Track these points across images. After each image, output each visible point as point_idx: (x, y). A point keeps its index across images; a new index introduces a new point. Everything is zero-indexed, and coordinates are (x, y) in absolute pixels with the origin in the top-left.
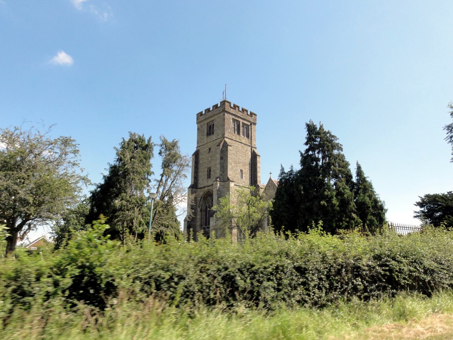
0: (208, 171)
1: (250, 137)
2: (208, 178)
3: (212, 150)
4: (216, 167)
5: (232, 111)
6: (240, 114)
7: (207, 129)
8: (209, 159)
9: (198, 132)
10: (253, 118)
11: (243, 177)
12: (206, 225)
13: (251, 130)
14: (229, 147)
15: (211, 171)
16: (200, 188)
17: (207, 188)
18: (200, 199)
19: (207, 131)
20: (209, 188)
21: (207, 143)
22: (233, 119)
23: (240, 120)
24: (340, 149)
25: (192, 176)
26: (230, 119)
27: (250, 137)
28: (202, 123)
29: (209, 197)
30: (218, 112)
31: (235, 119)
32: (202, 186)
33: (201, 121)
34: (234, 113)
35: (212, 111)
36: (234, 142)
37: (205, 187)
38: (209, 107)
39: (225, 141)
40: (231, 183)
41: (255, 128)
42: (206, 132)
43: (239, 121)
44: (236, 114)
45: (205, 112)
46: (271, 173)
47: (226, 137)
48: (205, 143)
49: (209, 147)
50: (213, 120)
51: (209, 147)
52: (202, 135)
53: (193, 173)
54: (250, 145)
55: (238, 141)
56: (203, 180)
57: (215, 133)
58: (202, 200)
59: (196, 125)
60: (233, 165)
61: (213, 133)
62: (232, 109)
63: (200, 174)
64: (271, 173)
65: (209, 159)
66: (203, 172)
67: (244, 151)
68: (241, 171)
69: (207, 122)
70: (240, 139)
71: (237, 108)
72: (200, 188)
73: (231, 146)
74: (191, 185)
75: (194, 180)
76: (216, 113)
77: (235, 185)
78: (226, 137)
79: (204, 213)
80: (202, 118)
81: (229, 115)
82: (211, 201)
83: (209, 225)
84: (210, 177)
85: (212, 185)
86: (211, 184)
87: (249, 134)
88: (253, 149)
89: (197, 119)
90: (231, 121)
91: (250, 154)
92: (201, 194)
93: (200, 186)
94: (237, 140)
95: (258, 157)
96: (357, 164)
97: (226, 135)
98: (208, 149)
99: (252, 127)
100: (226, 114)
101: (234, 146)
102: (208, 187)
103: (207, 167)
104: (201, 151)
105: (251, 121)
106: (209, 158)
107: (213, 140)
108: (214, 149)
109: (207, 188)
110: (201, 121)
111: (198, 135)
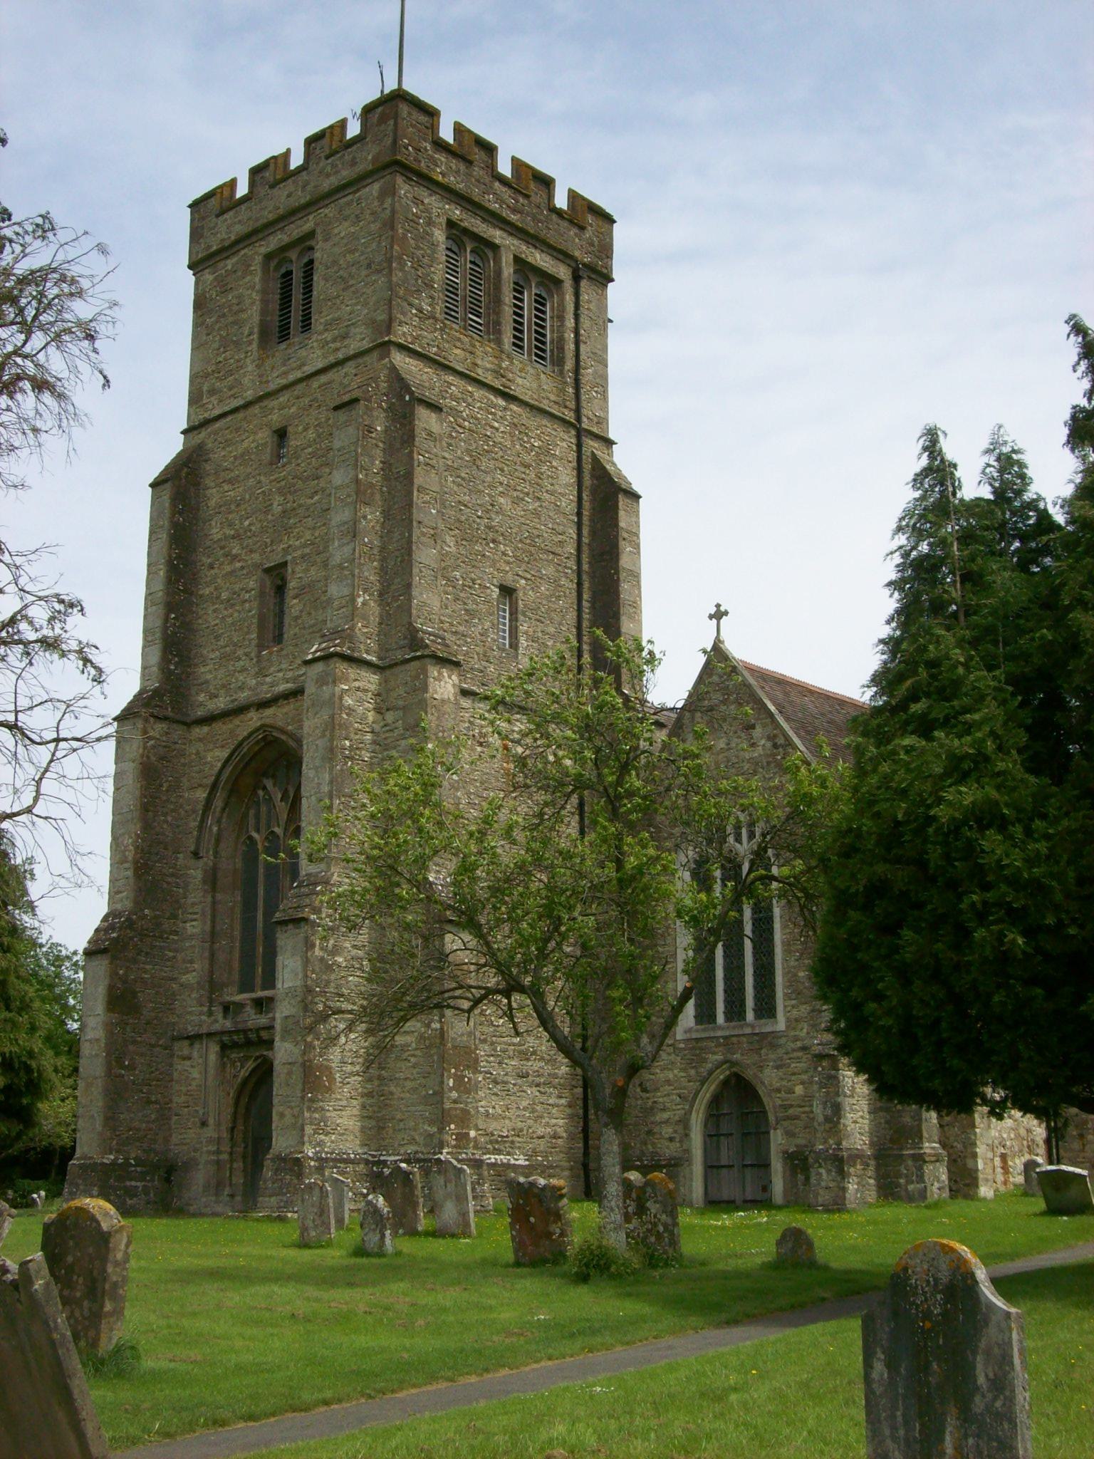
0: (262, 594)
1: (569, 364)
2: (261, 647)
3: (293, 442)
4: (325, 564)
5: (443, 169)
6: (500, 200)
7: (265, 302)
8: (277, 509)
9: (197, 324)
10: (588, 234)
11: (523, 642)
12: (246, 986)
13: (577, 317)
14: (422, 414)
15: (290, 593)
16: (209, 719)
17: (254, 719)
18: (202, 795)
19: (264, 312)
20: (269, 712)
21: (260, 399)
22: (451, 224)
23: (497, 236)
24: (1027, 468)
25: (147, 632)
26: (430, 222)
27: (569, 364)
28: (230, 263)
29: (269, 783)
30: (346, 174)
31: (465, 231)
32: (221, 703)
33: (226, 251)
34: (460, 187)
35: (300, 169)
36: (457, 386)
37: (241, 710)
38: (278, 150)
39: (393, 369)
40: (433, 671)
41: (603, 307)
42: (256, 319)
43: (495, 248)
44: (475, 193)
45: (252, 184)
46: (718, 615)
47: (402, 348)
48: (249, 395)
49: (277, 426)
50: (311, 235)
51: (276, 419)
52: (225, 344)
53: (160, 610)
54: (570, 416)
55: (489, 379)
56: (225, 657)
57: (318, 321)
58: (218, 803)
59: (190, 278)
60: (451, 545)
61: (306, 324)
62: (441, 157)
63: (210, 617)
64: (718, 615)
65: (277, 509)
66: (229, 603)
67: (527, 458)
68: (507, 592)
69: (263, 250)
70: (498, 373)
71: (478, 155)
72: (209, 719)
73: (436, 408)
74: (137, 697)
75: (165, 660)
76: (333, 181)
77: (465, 693)
78: (402, 348)
79: (231, 900)
80: (227, 228)
81: (423, 193)
82: (282, 809)
83: (270, 982)
84: (279, 638)
85: (297, 693)
86: (283, 687)
87: (560, 344)
88: (591, 445)
89: (196, 234)
90: (439, 235)
91: (567, 477)
92: (216, 756)
93: (35, 811)
94: (480, 374)
95: (621, 498)
96: (893, 538)
97: (402, 333)
98: (264, 436)
99: (584, 297)
100: (404, 189)
101: (455, 412)
102: (263, 705)
103: (256, 566)
104: (219, 455)
105: (577, 254)
106: (278, 499)
107: (309, 369)
108: (311, 434)
109: (254, 719)
110: (226, 251)
111: (197, 345)
